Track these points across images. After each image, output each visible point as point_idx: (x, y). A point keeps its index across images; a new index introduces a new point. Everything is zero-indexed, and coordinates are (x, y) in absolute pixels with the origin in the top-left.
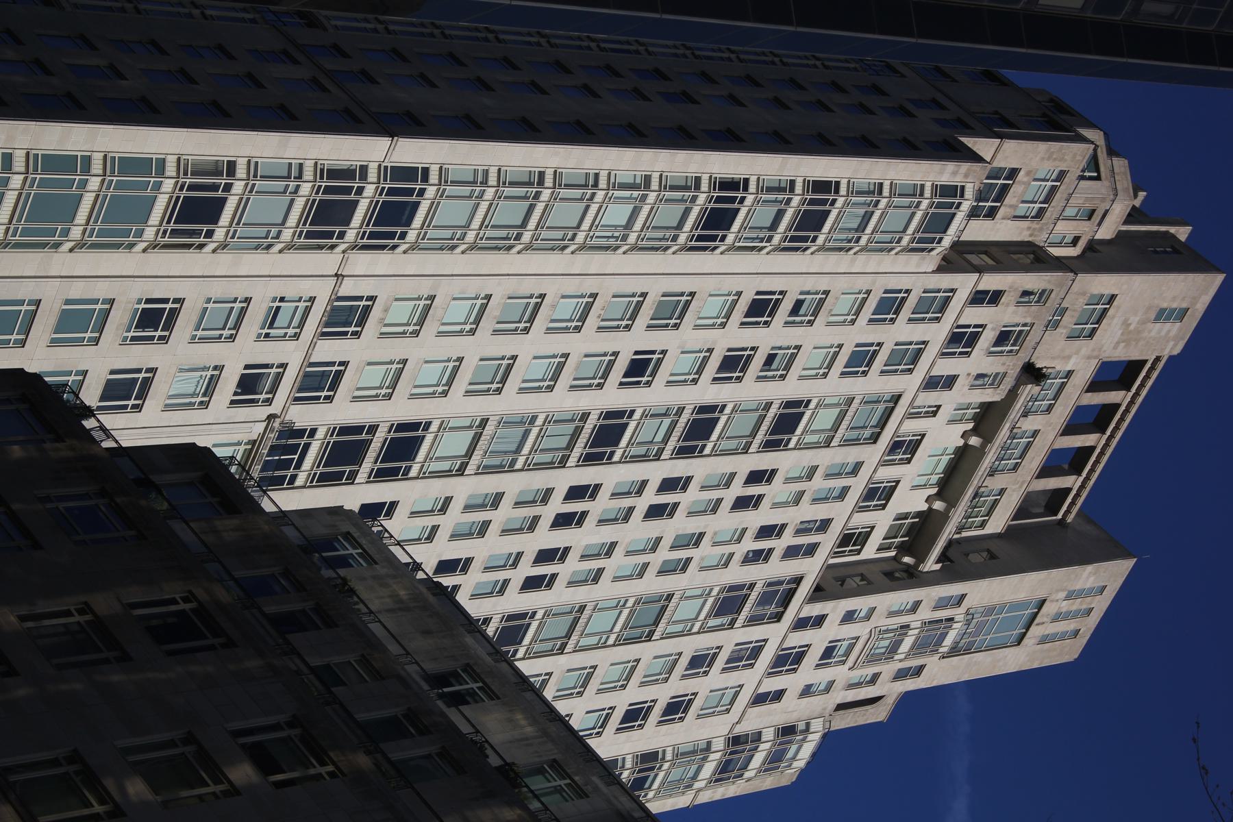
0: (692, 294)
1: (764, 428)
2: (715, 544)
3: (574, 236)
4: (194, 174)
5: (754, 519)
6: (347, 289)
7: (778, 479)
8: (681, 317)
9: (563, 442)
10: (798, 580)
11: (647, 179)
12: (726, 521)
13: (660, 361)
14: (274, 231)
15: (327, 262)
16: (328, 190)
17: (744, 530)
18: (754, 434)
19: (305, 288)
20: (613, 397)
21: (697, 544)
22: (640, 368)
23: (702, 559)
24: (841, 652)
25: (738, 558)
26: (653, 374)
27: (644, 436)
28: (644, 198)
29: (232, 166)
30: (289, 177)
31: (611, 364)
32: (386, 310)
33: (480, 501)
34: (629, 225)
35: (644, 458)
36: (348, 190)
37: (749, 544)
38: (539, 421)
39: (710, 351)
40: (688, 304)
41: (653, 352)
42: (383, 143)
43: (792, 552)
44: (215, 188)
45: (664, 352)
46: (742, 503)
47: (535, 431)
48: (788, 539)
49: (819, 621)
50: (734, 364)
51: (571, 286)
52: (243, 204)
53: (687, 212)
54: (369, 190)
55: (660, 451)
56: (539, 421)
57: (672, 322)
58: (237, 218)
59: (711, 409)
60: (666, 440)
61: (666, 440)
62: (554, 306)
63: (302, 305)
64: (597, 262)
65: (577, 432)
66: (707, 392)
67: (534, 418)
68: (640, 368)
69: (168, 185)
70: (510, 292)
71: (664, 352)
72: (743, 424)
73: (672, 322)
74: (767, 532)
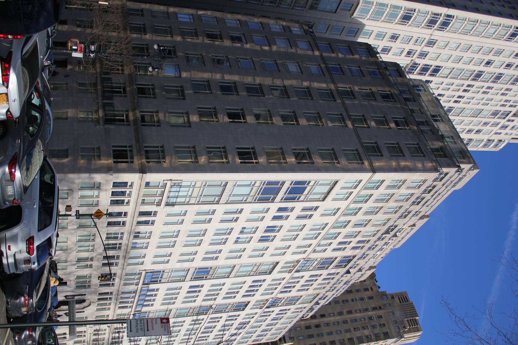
0: (504, 50)
1: (512, 80)
2: (495, 101)
3: (482, 34)
4: (407, 10)
5: (504, 98)
6: (432, 38)
7: (512, 91)
8: (500, 54)
9: (469, 75)
10: (511, 112)
11: (500, 24)
12: (499, 97)
13: (493, 62)
14: (420, 24)
15: (429, 31)
16: (433, 17)
17: (502, 100)
18: (509, 81)
19: (424, 36)
20: (482, 68)
21: (491, 101)
22: (488, 63)
23: (496, 99)
24: (516, 128)
25: (499, 105)
26: (491, 65)
27: (485, 77)
28: (499, 28)
29: (415, 10)
30: (426, 14)
31: (483, 61)
32: (439, 43)
33: (311, 208)
34: (494, 33)
35: (484, 81)
36: (437, 18)
37: (502, 103)
38: (465, 70)
39: (504, 62)
40: (502, 52)
41: (492, 60)
42: (446, 9)
43: (511, 106)
44: (411, 14)
45: (494, 61)
46: (503, 94)
47: (463, 72)
48: (511, 103)
49: (513, 121)
50: (509, 66)
51: (478, 44)
52: (416, 18)
53: (507, 32)
54: (441, 18)
55: (489, 81)
56: (465, 70)
57: (498, 55)
58: (414, 20)
59: (501, 74)
60: (490, 79)
61: (490, 79)
62: (474, 48)
63: (423, 39)
64: (485, 40)
65: (472, 74)
66: (502, 70)
67: (464, 69)
68: (488, 63)
69: (402, 12)
70: (498, 48)
71: (494, 61)
72: (508, 78)
73: (498, 55)
74: (506, 101)
